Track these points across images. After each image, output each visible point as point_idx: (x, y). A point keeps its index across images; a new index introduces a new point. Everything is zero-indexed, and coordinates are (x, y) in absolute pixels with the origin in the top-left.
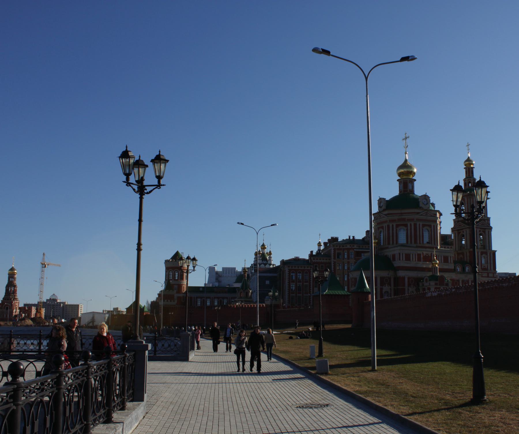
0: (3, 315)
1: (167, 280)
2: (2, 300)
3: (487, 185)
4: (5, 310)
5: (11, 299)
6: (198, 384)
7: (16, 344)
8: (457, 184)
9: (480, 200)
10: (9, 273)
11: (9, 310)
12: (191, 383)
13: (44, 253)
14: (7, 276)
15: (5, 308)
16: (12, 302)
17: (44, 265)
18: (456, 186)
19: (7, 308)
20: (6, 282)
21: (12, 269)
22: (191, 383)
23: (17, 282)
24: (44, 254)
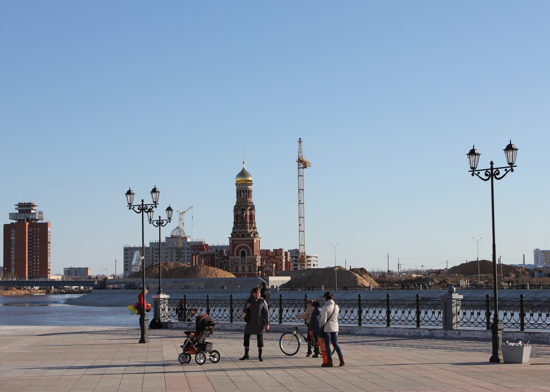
0: (237, 268)
1: (231, 243)
2: (230, 236)
3: (173, 209)
4: (240, 257)
5: (249, 235)
6: (124, 375)
7: (232, 328)
8: (169, 207)
9: (508, 152)
10: (237, 182)
11: (247, 257)
12: (123, 374)
13: (300, 139)
14: (235, 188)
15: (240, 254)
16: (253, 240)
17: (302, 163)
18: (168, 208)
19: (243, 254)
20: (233, 200)
21: (243, 174)
22: (123, 374)
23: (255, 199)
24: (300, 141)
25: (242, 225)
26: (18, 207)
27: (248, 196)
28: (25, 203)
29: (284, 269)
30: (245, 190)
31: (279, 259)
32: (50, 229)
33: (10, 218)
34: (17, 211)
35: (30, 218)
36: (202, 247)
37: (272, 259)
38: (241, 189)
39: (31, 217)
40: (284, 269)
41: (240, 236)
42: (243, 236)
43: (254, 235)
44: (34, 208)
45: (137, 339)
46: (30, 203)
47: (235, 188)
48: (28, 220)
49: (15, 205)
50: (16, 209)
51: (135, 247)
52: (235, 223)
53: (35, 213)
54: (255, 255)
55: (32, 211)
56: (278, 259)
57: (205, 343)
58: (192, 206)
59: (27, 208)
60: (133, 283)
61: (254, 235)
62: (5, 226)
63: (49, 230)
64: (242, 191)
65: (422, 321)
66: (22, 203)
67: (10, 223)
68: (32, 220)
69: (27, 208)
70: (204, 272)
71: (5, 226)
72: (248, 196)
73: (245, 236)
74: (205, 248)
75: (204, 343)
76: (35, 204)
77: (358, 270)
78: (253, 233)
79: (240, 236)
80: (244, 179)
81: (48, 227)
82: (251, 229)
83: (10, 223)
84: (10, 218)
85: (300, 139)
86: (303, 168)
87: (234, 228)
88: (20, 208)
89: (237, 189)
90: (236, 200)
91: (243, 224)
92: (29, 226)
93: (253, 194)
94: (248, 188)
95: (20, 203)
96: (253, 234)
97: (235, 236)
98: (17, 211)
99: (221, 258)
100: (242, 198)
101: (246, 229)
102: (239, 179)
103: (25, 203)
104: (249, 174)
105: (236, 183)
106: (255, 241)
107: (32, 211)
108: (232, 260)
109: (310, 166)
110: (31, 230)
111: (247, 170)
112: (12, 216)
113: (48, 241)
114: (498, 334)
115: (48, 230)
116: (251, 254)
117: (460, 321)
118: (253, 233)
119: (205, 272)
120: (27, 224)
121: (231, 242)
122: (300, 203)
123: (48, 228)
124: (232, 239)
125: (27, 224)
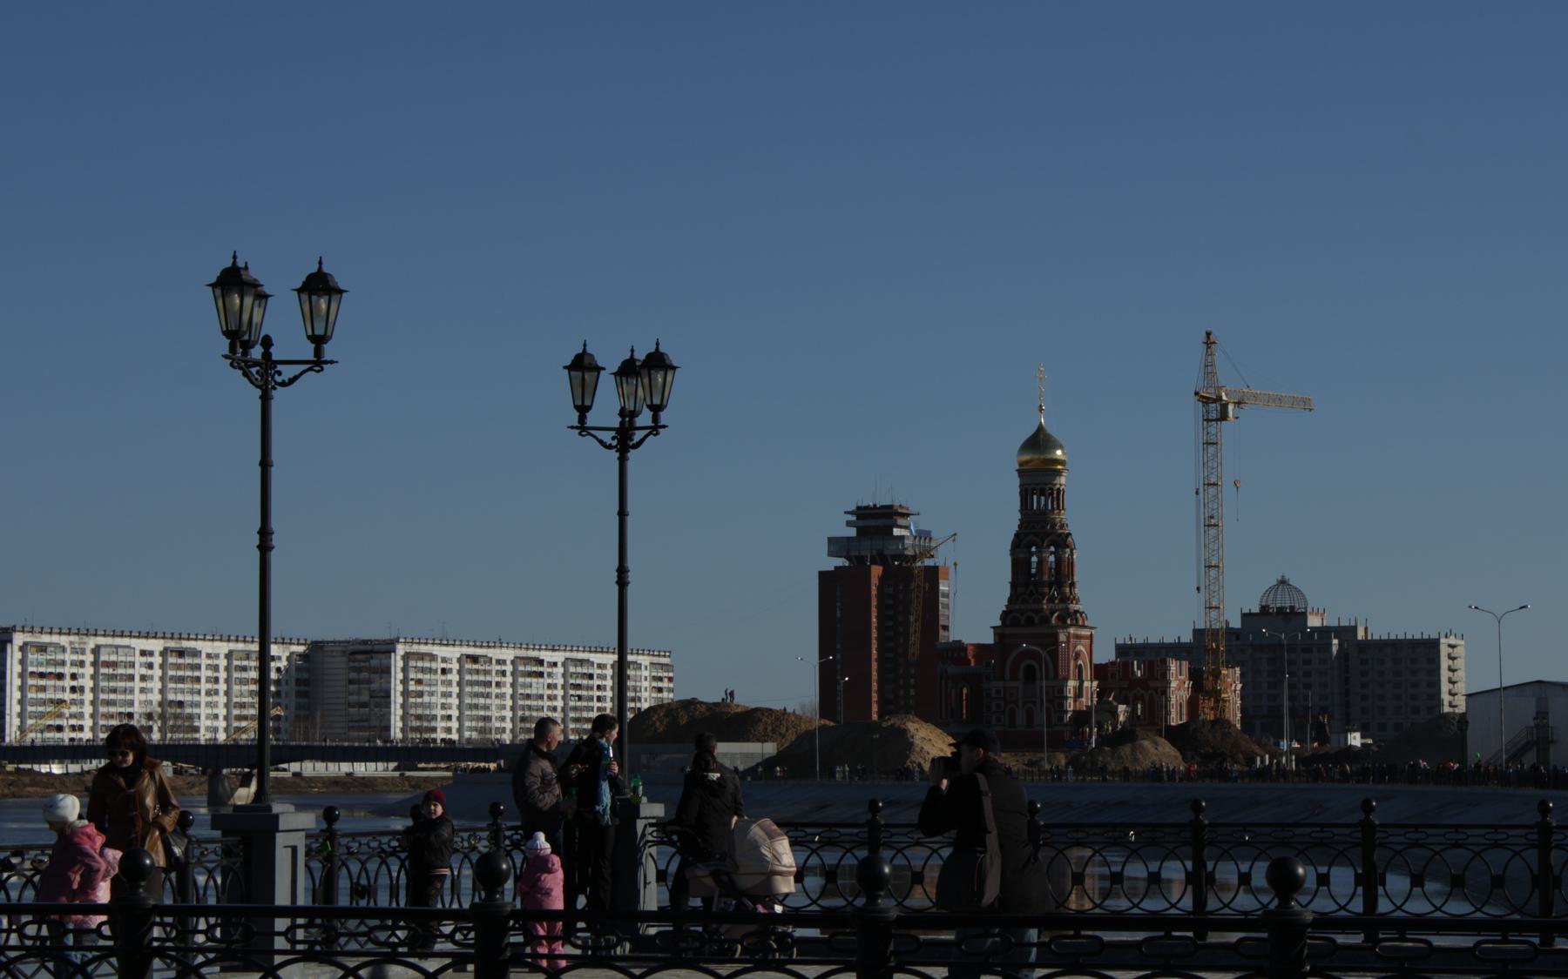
2: (999, 623)
10: (1021, 464)
13: (1208, 334)
15: (1021, 674)
16: (1056, 636)
17: (1214, 408)
19: (1030, 675)
21: (1039, 441)
23: (1074, 517)
24: (1209, 341)
25: (1029, 591)
26: (854, 518)
28: (875, 505)
31: (1159, 690)
32: (949, 587)
33: (831, 554)
34: (852, 532)
35: (887, 553)
36: (962, 654)
38: (1026, 487)
39: (890, 549)
41: (1023, 622)
42: (1030, 622)
43: (1062, 619)
44: (900, 521)
46: (891, 507)
47: (1017, 481)
48: (880, 558)
49: (846, 513)
50: (849, 524)
51: (1380, 640)
52: (1014, 585)
53: (902, 538)
54: (1060, 677)
55: (897, 532)
56: (1156, 689)
57: (360, 888)
58: (955, 534)
59: (880, 522)
61: (1062, 619)
62: (823, 575)
63: (943, 588)
65: (938, 845)
66: (867, 508)
67: (833, 569)
68: (896, 557)
69: (880, 522)
70: (766, 729)
71: (823, 575)
73: (1036, 621)
74: (970, 657)
76: (907, 509)
77: (1204, 726)
78: (1056, 614)
79: (1023, 622)
80: (1042, 457)
81: (940, 581)
82: (1053, 602)
83: (833, 569)
84: (831, 554)
85: (1208, 334)
86: (1217, 420)
87: (1010, 600)
88: (861, 523)
89: (1021, 486)
91: (1031, 587)
92: (882, 579)
93: (1068, 500)
94: (1056, 484)
95: (860, 505)
96: (1058, 617)
98: (852, 532)
99: (1125, 684)
101: (1040, 601)
102: (1026, 457)
103: (875, 505)
104: (1055, 441)
105: (1017, 467)
106: (1062, 637)
107: (897, 532)
108: (998, 692)
109: (1310, 410)
110: (891, 590)
111: (1050, 430)
112: (837, 546)
113: (941, 623)
115: (941, 588)
116: (1051, 675)
117: (939, 848)
118: (1056, 614)
119: (770, 728)
120: (876, 571)
122: (1208, 526)
123: (938, 583)
125: (876, 571)
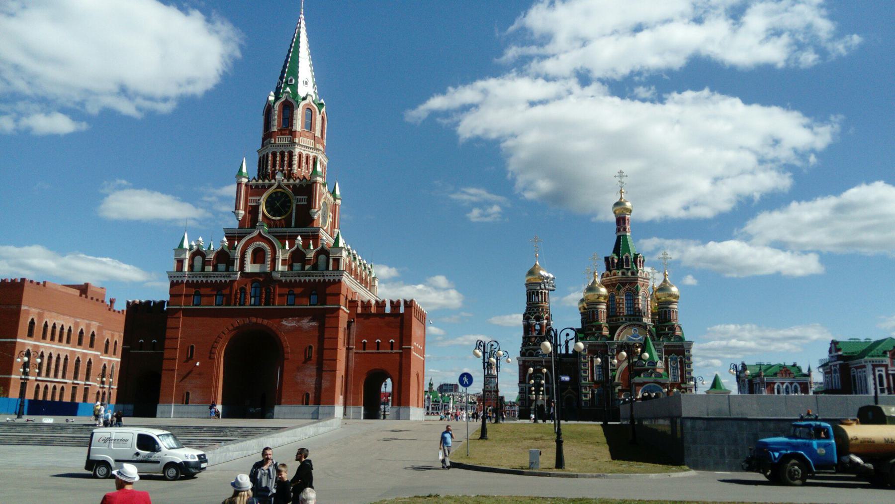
14: (525, 289)
27: (543, 301)
29: (609, 423)
30: (535, 291)
37: (673, 354)
40: (609, 423)
41: (535, 355)
45: (443, 425)
47: (526, 289)
60: (493, 135)
64: (531, 293)
72: (543, 301)
75: (763, 471)
79: (535, 355)
90: (526, 306)
97: (527, 354)
100: (531, 303)
114: (167, 330)
121: (521, 363)
124: (524, 358)
